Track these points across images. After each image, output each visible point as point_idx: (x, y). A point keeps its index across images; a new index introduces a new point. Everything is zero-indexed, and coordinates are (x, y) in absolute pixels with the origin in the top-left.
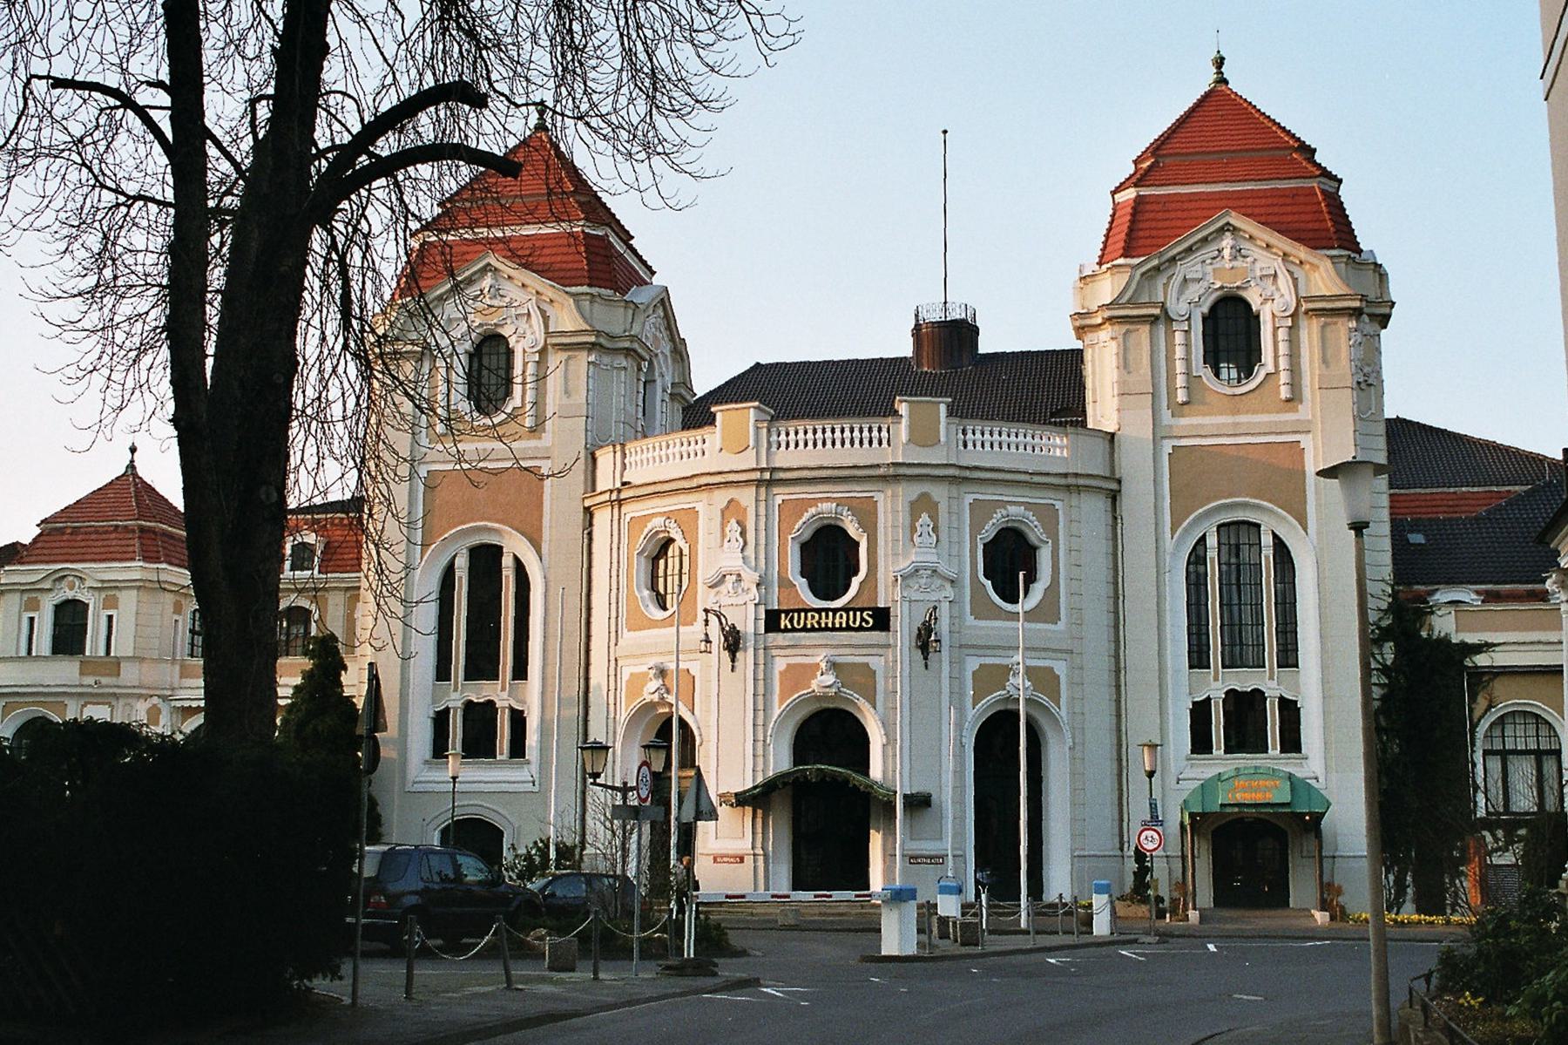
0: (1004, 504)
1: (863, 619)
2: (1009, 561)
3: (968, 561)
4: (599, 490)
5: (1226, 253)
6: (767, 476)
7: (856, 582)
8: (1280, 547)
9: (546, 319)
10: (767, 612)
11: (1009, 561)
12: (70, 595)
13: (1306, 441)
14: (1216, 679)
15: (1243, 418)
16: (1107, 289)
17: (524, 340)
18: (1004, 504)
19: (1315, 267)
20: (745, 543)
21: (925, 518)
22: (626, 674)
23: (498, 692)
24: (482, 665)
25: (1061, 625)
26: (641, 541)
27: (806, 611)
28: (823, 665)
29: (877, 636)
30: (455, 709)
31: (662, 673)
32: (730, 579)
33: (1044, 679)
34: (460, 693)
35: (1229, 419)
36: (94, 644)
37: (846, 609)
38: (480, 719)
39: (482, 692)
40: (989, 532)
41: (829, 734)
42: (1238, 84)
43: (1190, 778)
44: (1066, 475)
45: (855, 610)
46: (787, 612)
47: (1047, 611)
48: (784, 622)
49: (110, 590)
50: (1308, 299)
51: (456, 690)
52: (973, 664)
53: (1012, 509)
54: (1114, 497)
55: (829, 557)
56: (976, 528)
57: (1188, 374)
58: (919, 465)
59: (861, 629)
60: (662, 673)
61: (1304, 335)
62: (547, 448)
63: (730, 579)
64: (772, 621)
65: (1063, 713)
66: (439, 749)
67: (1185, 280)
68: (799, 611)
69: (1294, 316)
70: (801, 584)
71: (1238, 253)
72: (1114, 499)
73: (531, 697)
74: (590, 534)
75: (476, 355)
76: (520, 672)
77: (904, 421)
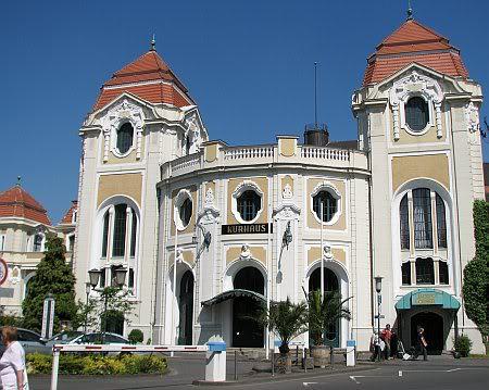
2: (326, 203)
3: (305, 203)
11: (326, 203)
17: (139, 122)
40: (315, 191)
52: (308, 247)
76: (133, 253)
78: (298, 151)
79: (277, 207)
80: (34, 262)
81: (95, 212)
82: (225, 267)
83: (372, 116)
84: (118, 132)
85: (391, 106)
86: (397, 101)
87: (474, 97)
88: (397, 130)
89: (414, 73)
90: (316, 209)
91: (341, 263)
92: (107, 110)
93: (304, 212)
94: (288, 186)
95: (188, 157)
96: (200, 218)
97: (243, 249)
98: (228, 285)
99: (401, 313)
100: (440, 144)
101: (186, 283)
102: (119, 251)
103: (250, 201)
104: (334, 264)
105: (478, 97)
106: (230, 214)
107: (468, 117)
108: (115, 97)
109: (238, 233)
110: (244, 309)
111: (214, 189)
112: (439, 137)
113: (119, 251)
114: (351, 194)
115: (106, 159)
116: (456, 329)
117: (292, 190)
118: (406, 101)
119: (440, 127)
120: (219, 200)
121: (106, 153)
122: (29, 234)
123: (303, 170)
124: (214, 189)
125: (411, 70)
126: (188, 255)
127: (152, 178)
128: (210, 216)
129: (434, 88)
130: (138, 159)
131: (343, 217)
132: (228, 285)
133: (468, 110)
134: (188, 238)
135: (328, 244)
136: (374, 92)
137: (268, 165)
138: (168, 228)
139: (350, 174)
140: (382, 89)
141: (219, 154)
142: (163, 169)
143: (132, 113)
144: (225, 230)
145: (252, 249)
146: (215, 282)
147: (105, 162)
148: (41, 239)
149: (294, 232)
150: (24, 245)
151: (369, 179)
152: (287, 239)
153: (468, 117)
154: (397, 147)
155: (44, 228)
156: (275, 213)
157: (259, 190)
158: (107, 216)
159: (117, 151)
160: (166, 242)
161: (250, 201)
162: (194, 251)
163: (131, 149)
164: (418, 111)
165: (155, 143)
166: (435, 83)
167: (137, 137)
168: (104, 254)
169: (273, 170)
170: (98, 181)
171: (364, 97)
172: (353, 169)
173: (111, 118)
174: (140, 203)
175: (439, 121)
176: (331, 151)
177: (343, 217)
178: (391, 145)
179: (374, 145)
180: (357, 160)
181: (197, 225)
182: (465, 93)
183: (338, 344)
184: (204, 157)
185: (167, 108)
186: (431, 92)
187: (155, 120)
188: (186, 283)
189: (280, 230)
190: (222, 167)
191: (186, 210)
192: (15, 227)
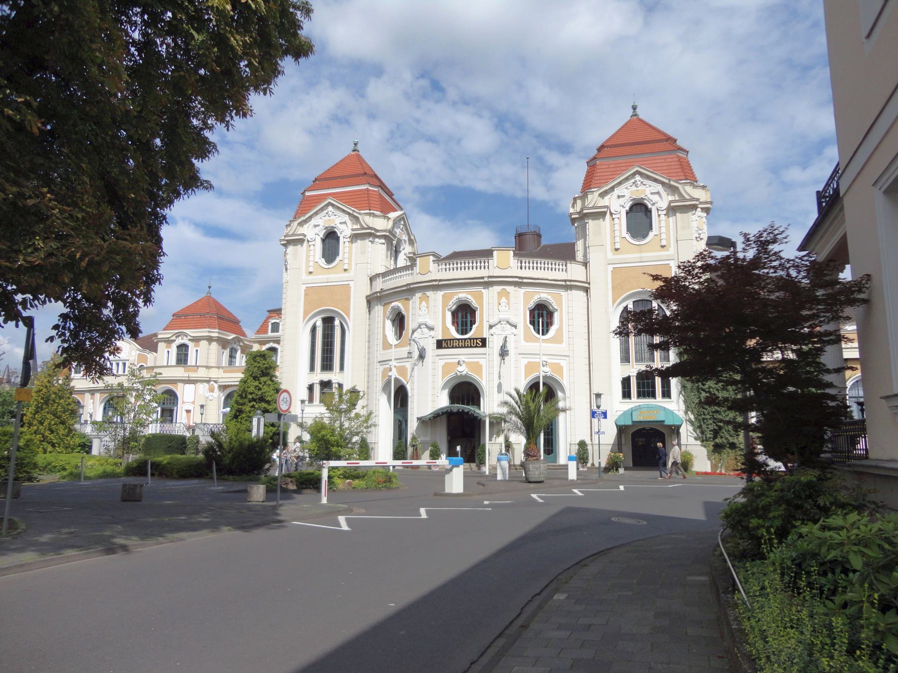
2: (541, 316)
3: (522, 317)
11: (541, 316)
12: (182, 342)
17: (345, 230)
21: (504, 300)
25: (564, 345)
34: (320, 376)
35: (638, 255)
36: (191, 361)
37: (470, 339)
40: (532, 304)
41: (465, 392)
42: (642, 116)
43: (618, 407)
44: (565, 281)
46: (445, 340)
48: (444, 344)
49: (196, 340)
52: (524, 362)
59: (476, 347)
64: (440, 344)
72: (587, 291)
76: (342, 368)
78: (513, 262)
79: (492, 322)
80: (235, 377)
81: (301, 325)
82: (440, 382)
83: (591, 224)
84: (323, 240)
85: (611, 214)
86: (619, 209)
87: (701, 203)
88: (617, 239)
89: (638, 178)
90: (532, 322)
91: (475, 376)
92: (311, 217)
93: (521, 326)
94: (424, 303)
95: (397, 270)
96: (413, 332)
97: (459, 363)
98: (443, 401)
99: (621, 430)
100: (663, 253)
101: (401, 397)
102: (327, 365)
103: (464, 315)
104: (551, 378)
105: (706, 203)
106: (445, 329)
107: (695, 224)
108: (315, 206)
109: (453, 347)
110: (461, 427)
111: (427, 303)
112: (663, 247)
113: (327, 365)
114: (568, 308)
115: (311, 270)
116: (679, 445)
117: (508, 304)
118: (627, 208)
119: (664, 236)
120: (431, 315)
121: (311, 264)
122: (224, 347)
123: (437, 286)
124: (427, 303)
125: (634, 174)
126: (402, 370)
127: (360, 292)
128: (425, 330)
129: (658, 193)
130: (345, 270)
131: (560, 329)
132: (443, 401)
133: (695, 217)
134: (403, 351)
135: (545, 358)
136: (593, 199)
137: (483, 278)
138: (380, 341)
139: (568, 286)
140: (603, 195)
141: (433, 267)
142: (372, 279)
143: (648, 191)
144: (440, 344)
145: (468, 364)
146: (430, 398)
147: (311, 273)
148: (236, 351)
149: (510, 347)
150: (219, 360)
151: (587, 290)
152: (504, 353)
153: (695, 224)
154: (618, 257)
155: (239, 340)
156: (491, 327)
157: (474, 304)
158: (314, 329)
159: (322, 262)
160: (381, 354)
161: (464, 315)
162: (408, 365)
163: (338, 259)
164: (641, 215)
165: (363, 253)
166: (659, 188)
167: (344, 246)
168: (312, 368)
169: (488, 284)
170: (303, 293)
171: (583, 203)
172: (570, 281)
173: (315, 226)
174: (349, 316)
175: (663, 230)
176: (541, 262)
177: (560, 329)
178: (610, 255)
179: (593, 257)
180: (575, 272)
181: (412, 340)
182: (693, 199)
183: (555, 459)
184: (417, 269)
185: (374, 216)
186: (655, 198)
187: (364, 228)
188: (401, 397)
189: (495, 344)
190: (435, 281)
191: (399, 321)
192: (210, 340)
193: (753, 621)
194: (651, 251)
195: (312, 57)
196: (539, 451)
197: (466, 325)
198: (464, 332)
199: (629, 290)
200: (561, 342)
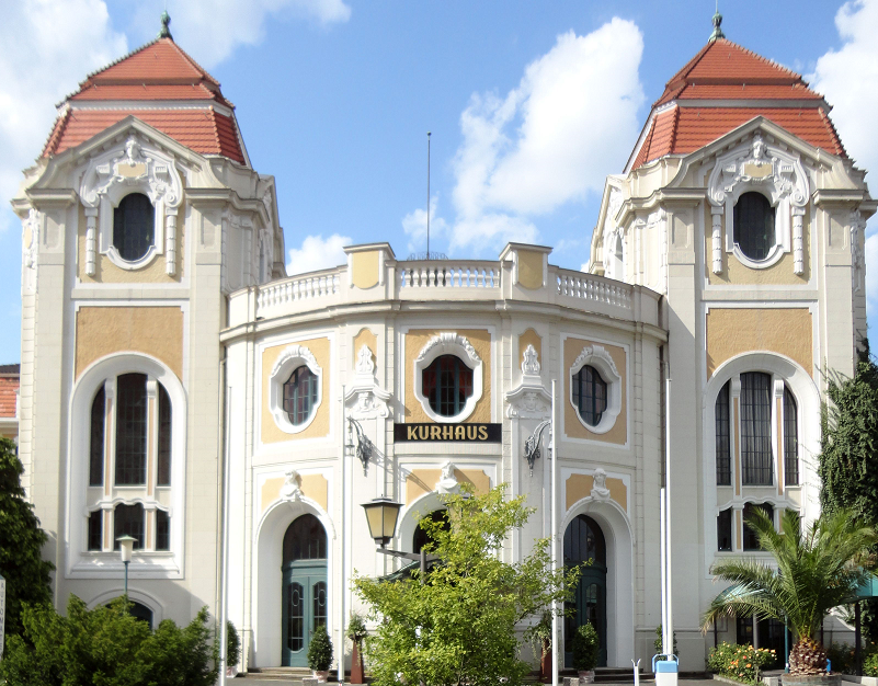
0: (590, 343)
1: (479, 433)
4: (233, 323)
5: (756, 152)
6: (397, 308)
7: (471, 403)
8: (788, 393)
9: (184, 179)
10: (396, 426)
13: (185, 306)
14: (738, 493)
15: (765, 288)
16: (660, 176)
17: (164, 198)
18: (590, 343)
19: (829, 167)
20: (375, 367)
21: (530, 348)
22: (260, 481)
23: (144, 495)
24: (130, 472)
25: (627, 446)
26: (274, 369)
27: (430, 425)
28: (447, 471)
29: (490, 448)
30: (107, 510)
31: (297, 479)
32: (363, 397)
33: (617, 488)
37: (465, 424)
38: (129, 520)
39: (128, 495)
40: (576, 368)
45: (472, 425)
46: (413, 425)
47: (617, 435)
48: (411, 433)
50: (823, 192)
51: (107, 493)
52: (567, 473)
53: (596, 348)
54: (662, 348)
55: (446, 381)
56: (569, 361)
57: (722, 250)
58: (594, 314)
59: (477, 440)
60: (297, 479)
61: (813, 227)
62: (187, 290)
63: (363, 397)
64: (401, 433)
65: (629, 514)
66: (94, 541)
67: (722, 174)
68: (424, 425)
69: (807, 207)
70: (424, 403)
71: (765, 154)
73: (173, 500)
74: (225, 365)
75: (119, 213)
76: (164, 478)
77: (514, 268)
113: (130, 472)
131: (622, 418)
144: (401, 433)
193: (466, 595)
194: (778, 282)
195: (312, 502)
196: (109, 353)
197: (452, 399)
198: (449, 410)
199: (736, 351)
200: (623, 441)
